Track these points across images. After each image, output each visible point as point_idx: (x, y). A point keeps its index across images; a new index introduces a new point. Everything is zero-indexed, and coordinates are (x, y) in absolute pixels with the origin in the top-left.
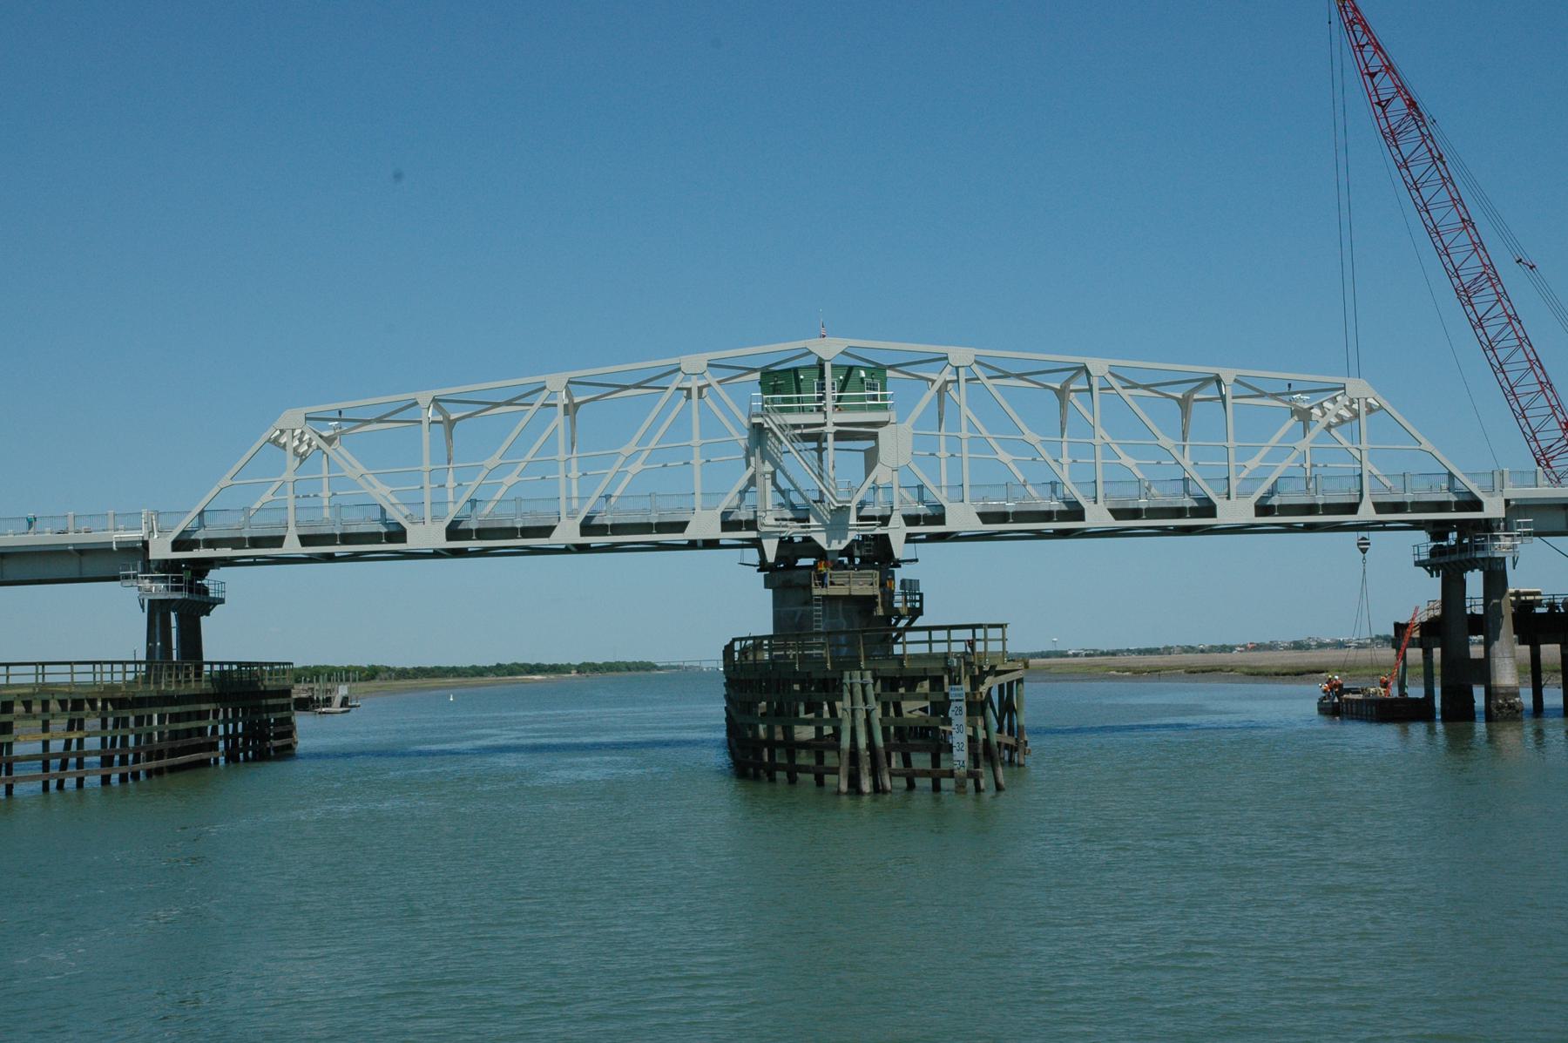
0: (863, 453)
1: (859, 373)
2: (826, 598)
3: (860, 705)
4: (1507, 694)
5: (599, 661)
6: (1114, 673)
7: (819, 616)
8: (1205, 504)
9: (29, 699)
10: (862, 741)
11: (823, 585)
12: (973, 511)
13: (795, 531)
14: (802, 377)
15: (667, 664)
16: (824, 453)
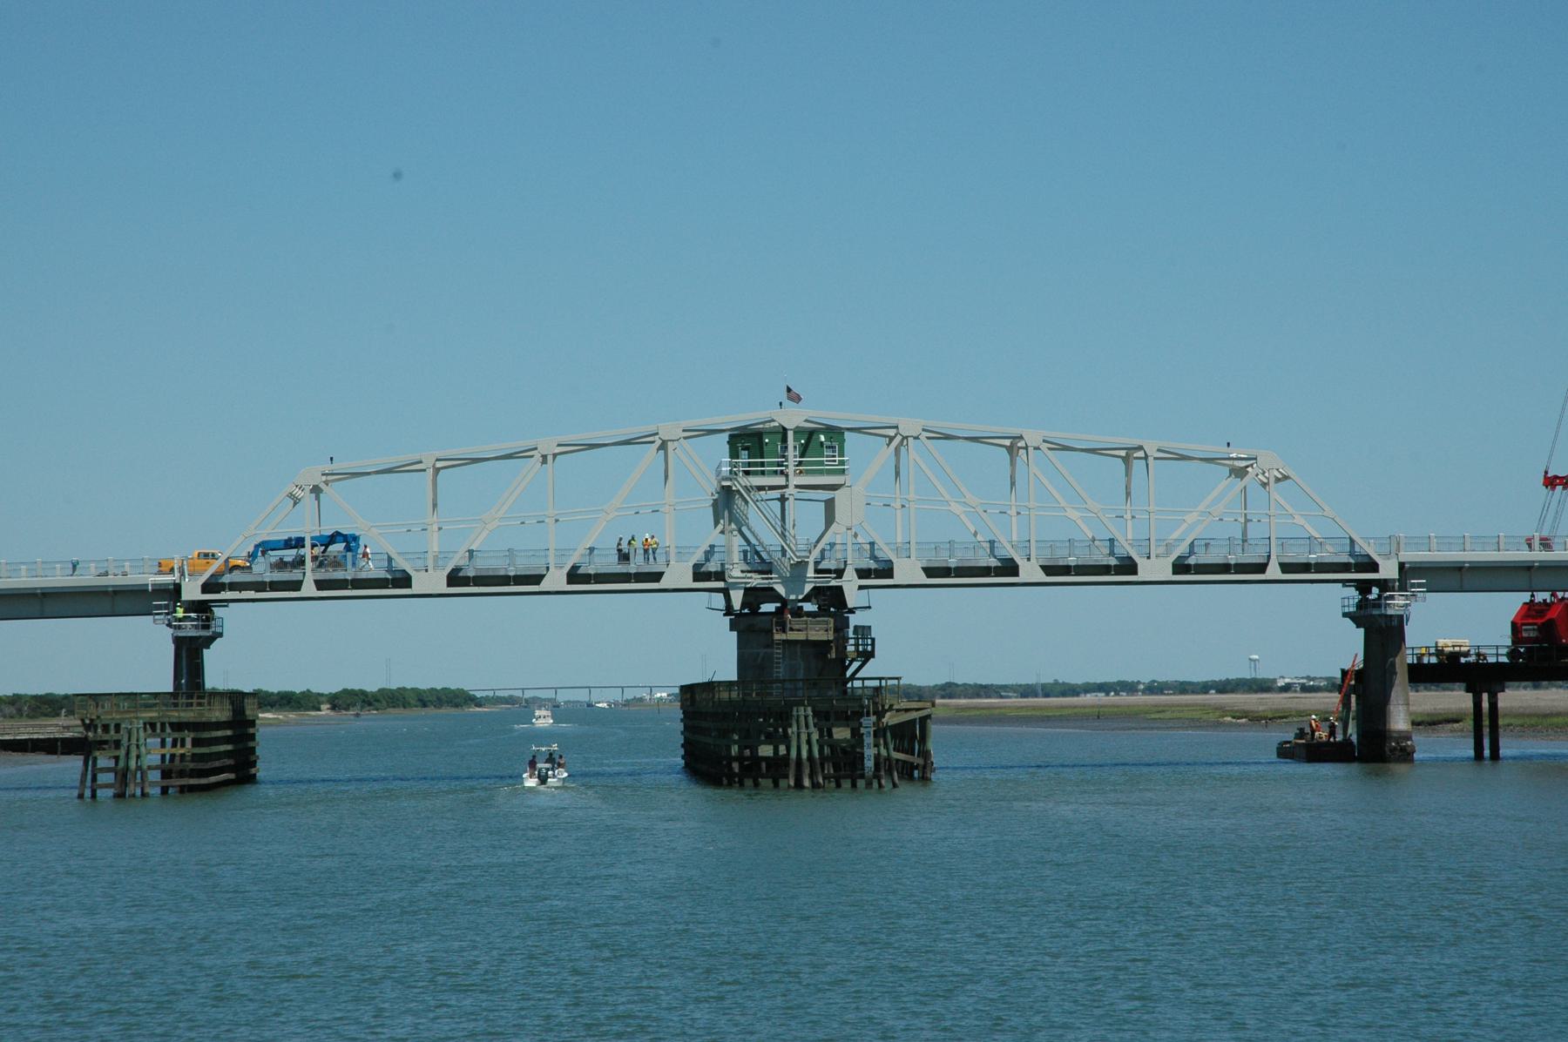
0: (823, 503)
1: (819, 438)
2: (786, 642)
3: (803, 730)
4: (1400, 738)
5: (371, 687)
6: (1229, 719)
7: (779, 658)
8: (1127, 562)
9: (107, 722)
10: (804, 754)
11: (784, 631)
12: (920, 565)
13: (756, 581)
14: (767, 441)
15: (491, 694)
16: (787, 503)
